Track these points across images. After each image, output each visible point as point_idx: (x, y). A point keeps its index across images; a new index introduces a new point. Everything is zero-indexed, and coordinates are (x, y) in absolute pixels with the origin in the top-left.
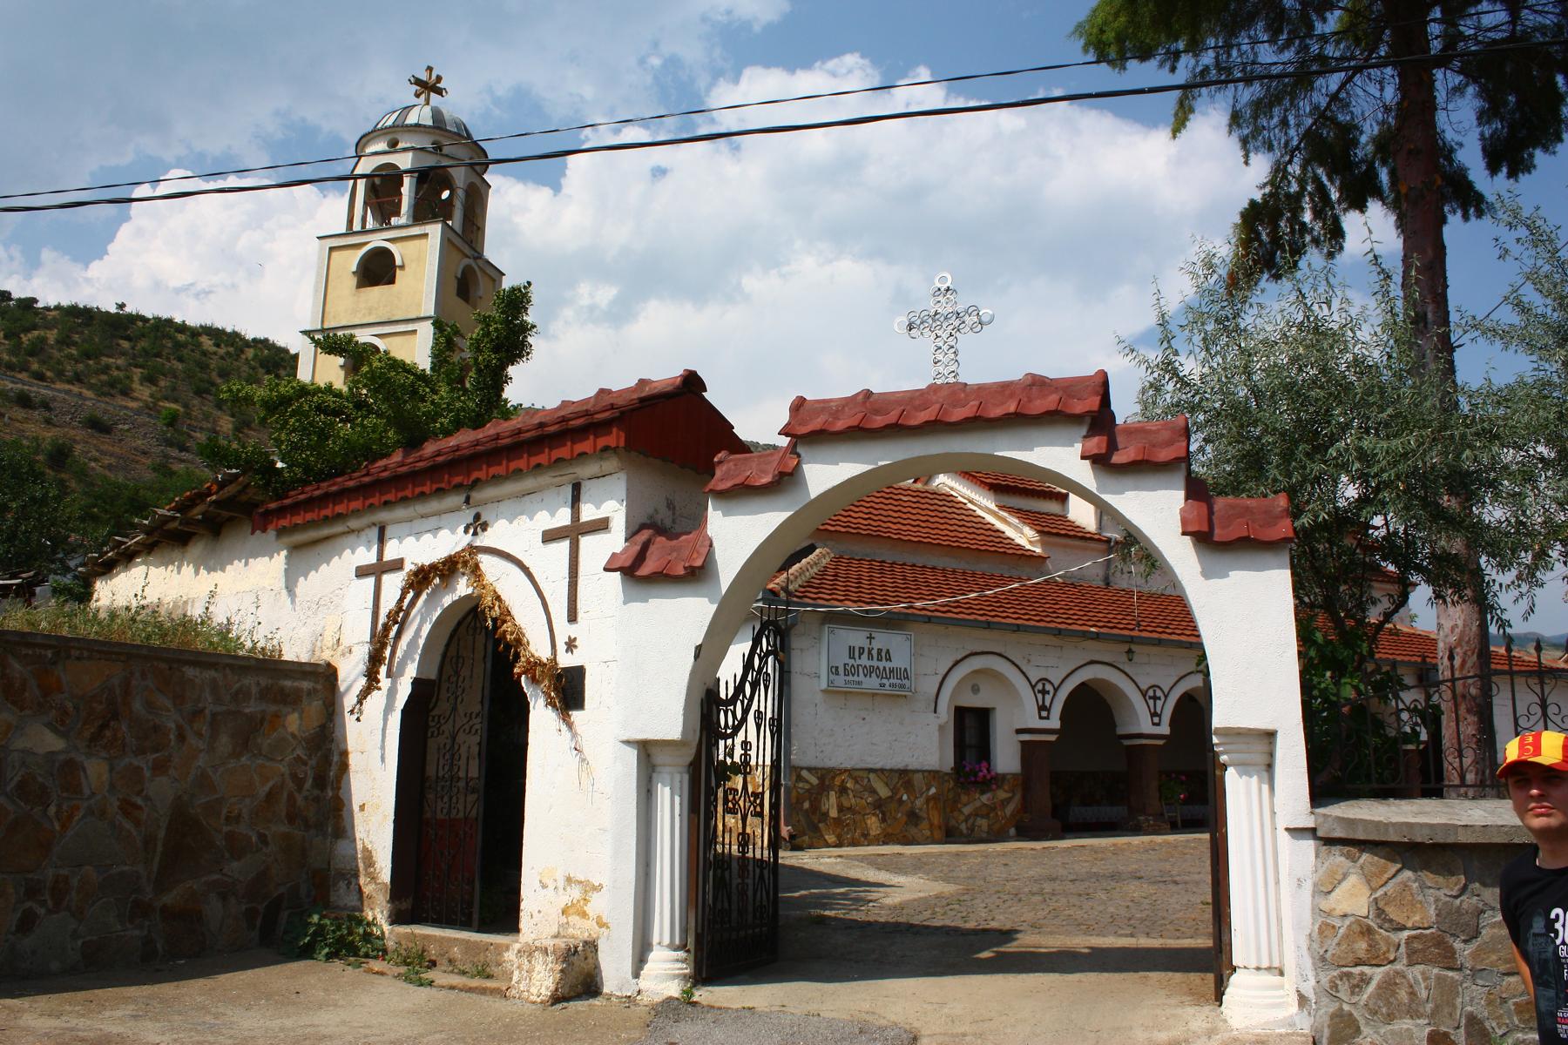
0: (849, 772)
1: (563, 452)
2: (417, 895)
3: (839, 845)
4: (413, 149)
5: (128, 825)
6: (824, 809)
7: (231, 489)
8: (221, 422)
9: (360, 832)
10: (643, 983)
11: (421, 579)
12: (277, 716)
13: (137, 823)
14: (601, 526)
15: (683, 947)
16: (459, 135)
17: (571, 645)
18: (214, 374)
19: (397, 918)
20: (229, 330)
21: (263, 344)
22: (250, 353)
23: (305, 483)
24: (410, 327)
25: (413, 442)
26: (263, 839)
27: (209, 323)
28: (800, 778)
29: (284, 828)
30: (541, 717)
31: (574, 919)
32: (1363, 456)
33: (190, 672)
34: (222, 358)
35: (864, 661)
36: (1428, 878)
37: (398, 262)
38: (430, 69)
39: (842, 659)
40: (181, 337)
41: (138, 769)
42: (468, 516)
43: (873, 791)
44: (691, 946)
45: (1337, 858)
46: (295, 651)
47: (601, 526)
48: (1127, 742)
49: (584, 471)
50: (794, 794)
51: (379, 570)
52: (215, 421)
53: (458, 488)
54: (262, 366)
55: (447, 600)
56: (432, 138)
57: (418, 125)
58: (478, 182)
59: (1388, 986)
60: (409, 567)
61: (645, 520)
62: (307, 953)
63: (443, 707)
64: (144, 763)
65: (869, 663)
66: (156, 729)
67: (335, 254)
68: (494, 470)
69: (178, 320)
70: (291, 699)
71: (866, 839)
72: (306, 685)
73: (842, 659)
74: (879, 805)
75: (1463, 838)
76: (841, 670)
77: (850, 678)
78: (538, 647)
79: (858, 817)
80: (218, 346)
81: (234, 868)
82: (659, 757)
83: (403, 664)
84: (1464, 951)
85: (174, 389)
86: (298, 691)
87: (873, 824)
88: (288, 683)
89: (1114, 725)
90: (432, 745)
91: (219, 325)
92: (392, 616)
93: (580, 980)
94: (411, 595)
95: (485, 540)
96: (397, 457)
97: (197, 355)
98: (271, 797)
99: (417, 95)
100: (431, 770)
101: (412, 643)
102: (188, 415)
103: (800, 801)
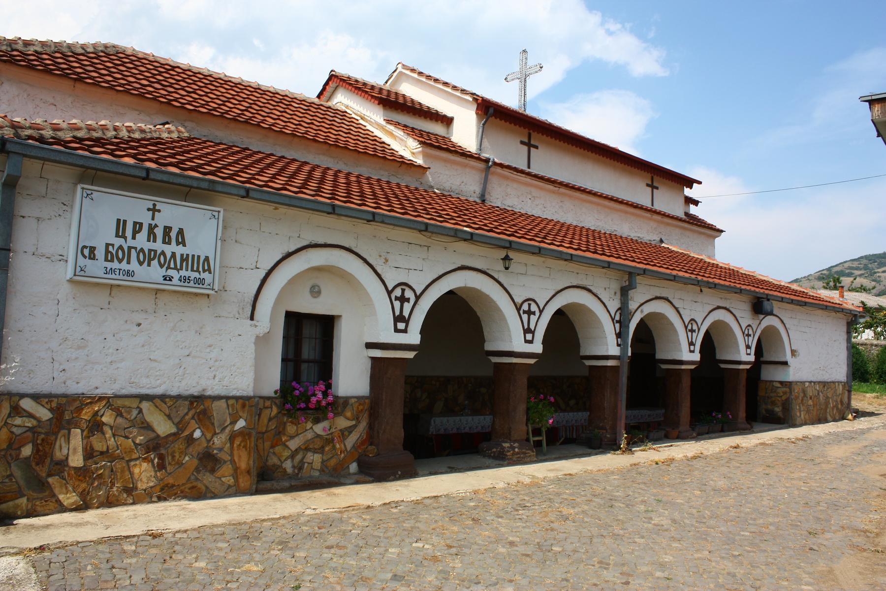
0: (108, 401)
3: (83, 507)
6: (59, 455)
28: (16, 410)
39: (105, 235)
43: (147, 427)
65: (148, 246)
73: (105, 235)
74: (155, 447)
76: (100, 253)
77: (115, 265)
79: (118, 465)
87: (144, 473)
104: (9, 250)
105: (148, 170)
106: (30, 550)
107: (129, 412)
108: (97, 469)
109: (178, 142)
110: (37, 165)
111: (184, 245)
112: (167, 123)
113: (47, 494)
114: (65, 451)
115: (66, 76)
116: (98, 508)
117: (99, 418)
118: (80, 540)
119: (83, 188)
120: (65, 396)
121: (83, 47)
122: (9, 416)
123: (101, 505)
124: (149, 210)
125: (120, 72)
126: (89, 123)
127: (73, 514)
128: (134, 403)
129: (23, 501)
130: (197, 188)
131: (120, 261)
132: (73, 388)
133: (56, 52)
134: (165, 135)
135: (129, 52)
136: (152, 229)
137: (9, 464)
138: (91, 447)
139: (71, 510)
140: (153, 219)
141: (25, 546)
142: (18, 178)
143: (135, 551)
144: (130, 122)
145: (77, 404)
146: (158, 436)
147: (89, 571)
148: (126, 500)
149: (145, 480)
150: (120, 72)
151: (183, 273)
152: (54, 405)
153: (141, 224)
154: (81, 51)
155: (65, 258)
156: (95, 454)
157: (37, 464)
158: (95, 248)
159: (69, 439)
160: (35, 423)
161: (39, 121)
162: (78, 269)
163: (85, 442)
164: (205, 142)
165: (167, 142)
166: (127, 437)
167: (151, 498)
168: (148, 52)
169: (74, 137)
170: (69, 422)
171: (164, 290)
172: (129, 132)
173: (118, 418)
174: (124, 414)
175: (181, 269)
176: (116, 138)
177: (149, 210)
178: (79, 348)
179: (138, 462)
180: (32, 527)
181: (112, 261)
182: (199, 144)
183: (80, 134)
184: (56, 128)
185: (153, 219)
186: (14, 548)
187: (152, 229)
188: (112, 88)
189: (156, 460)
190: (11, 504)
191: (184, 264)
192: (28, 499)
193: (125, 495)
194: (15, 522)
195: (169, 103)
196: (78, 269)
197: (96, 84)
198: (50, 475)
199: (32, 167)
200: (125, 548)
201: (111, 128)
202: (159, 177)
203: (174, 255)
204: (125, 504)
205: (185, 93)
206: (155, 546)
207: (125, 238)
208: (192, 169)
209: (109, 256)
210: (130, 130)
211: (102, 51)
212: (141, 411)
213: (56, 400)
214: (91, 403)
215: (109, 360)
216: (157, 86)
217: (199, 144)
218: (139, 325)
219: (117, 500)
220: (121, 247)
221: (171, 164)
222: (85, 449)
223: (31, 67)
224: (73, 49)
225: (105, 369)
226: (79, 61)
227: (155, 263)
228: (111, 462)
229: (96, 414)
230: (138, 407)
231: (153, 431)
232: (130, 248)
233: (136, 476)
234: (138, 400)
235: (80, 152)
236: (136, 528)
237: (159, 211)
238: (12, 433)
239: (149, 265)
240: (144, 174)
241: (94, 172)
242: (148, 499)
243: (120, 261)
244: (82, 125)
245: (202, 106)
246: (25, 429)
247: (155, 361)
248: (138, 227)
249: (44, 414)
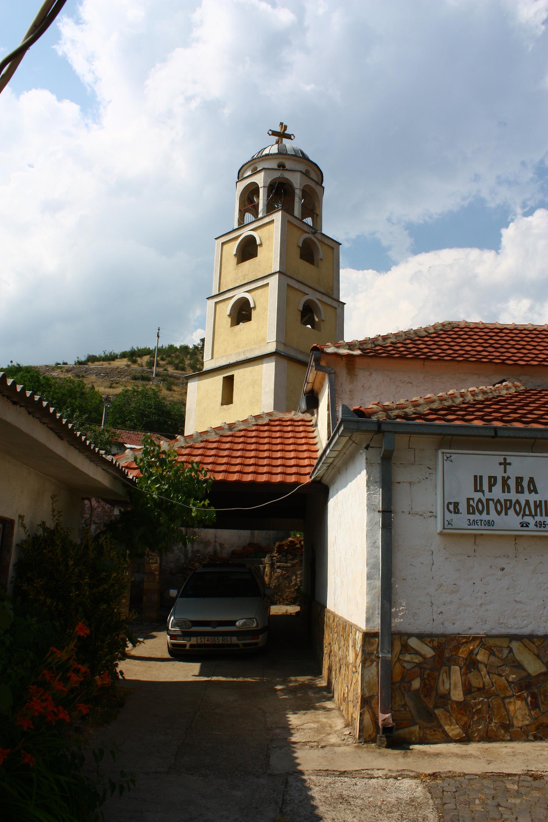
0: (483, 641)
3: (465, 739)
4: (264, 169)
6: (442, 689)
16: (297, 156)
28: (406, 648)
32: (461, 784)
35: (497, 493)
37: (258, 242)
39: (465, 491)
43: (518, 666)
50: (397, 669)
65: (503, 497)
67: (225, 247)
73: (465, 491)
74: (527, 685)
76: (463, 507)
77: (477, 516)
79: (495, 702)
87: (519, 711)
103: (406, 677)
104: (391, 512)
105: (496, 429)
106: (426, 776)
107: (501, 651)
108: (476, 705)
109: (516, 396)
110: (406, 438)
111: (536, 493)
112: (504, 381)
113: (435, 724)
114: (447, 686)
115: (416, 358)
116: (479, 741)
117: (474, 656)
118: (466, 772)
119: (443, 453)
120: (444, 636)
121: (426, 330)
122: (401, 653)
123: (482, 739)
124: (500, 464)
125: (458, 344)
126: (440, 394)
127: (458, 745)
128: (504, 643)
129: (416, 728)
130: (541, 438)
131: (481, 513)
132: (451, 629)
133: (406, 339)
134: (504, 392)
135: (462, 325)
136: (505, 481)
137: (403, 694)
138: (470, 684)
139: (456, 741)
140: (505, 472)
141: (421, 771)
142: (392, 452)
143: (517, 791)
144: (471, 387)
145: (455, 643)
146: (529, 675)
147: (477, 806)
148: (504, 736)
149: (520, 717)
150: (458, 344)
151: (538, 518)
152: (435, 644)
153: (495, 478)
154: (425, 334)
155: (434, 514)
156: (473, 690)
157: (425, 696)
158: (458, 503)
159: (450, 675)
160: (421, 659)
161: (402, 401)
162: (446, 523)
163: (464, 678)
164: (540, 392)
165: (508, 398)
166: (500, 675)
167: (528, 736)
168: (477, 321)
169: (430, 409)
170: (449, 659)
171: (522, 536)
172: (473, 395)
173: (491, 657)
174: (496, 653)
175: (536, 515)
176: (463, 403)
177: (500, 464)
178: (453, 592)
179: (512, 700)
180: (425, 754)
181: (474, 513)
182: (535, 395)
183: (435, 406)
184: (416, 404)
185: (505, 472)
186: (412, 771)
187: (505, 481)
188: (453, 360)
189: (529, 699)
190: (406, 730)
191: (538, 510)
192: (420, 728)
193: (503, 732)
194: (411, 747)
195: (503, 363)
196: (446, 523)
197: (441, 360)
198: (436, 707)
199: (402, 440)
200: (508, 786)
201: (458, 395)
202: (506, 433)
203: (527, 502)
204: (503, 740)
205: (515, 351)
206: (537, 789)
207: (483, 492)
208: (535, 421)
209: (471, 510)
210: (473, 394)
211: (441, 330)
212: (511, 651)
213: (436, 639)
214: (466, 642)
215: (479, 602)
216: (490, 349)
217: (535, 395)
218: (503, 569)
219: (496, 736)
220: (480, 500)
221: (515, 420)
222: (464, 685)
223: (390, 357)
224: (419, 334)
225: (476, 611)
226: (424, 343)
227: (511, 512)
228: (488, 698)
229: (471, 652)
230: (508, 647)
231: (524, 669)
232: (488, 500)
233: (512, 714)
234: (507, 640)
235: (437, 422)
236: (515, 767)
237: (510, 464)
238: (404, 667)
239: (506, 514)
240: (492, 433)
241: (451, 437)
242: (525, 737)
243: (481, 513)
244: (435, 398)
245: (533, 359)
246: (413, 665)
247: (520, 602)
248: (493, 481)
249: (428, 652)
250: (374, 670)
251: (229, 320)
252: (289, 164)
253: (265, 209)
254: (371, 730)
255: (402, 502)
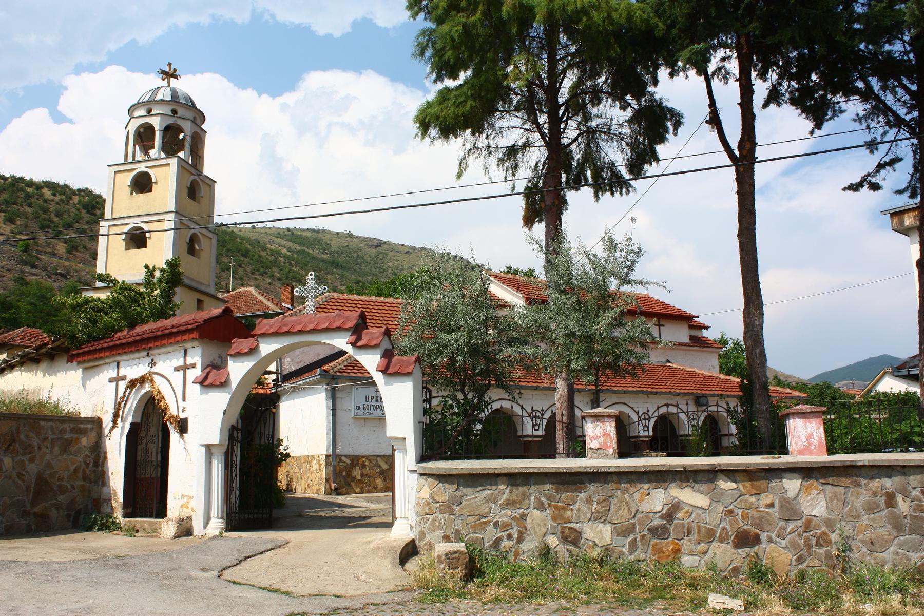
1: (179, 339)
2: (133, 507)
3: (362, 493)
5: (20, 482)
6: (354, 475)
7: (58, 343)
8: (58, 248)
9: (112, 484)
10: (207, 531)
11: (132, 384)
12: (77, 439)
13: (23, 481)
14: (193, 366)
15: (222, 518)
17: (184, 410)
18: (53, 214)
19: (126, 515)
20: (61, 183)
21: (85, 192)
22: (76, 199)
23: (88, 342)
24: (161, 217)
25: (132, 326)
26: (73, 487)
27: (48, 179)
28: (341, 460)
29: (81, 483)
30: (174, 436)
31: (185, 509)
33: (42, 423)
34: (58, 203)
36: (447, 485)
37: (154, 180)
38: (170, 64)
40: (30, 190)
41: (23, 461)
42: (149, 360)
43: (380, 466)
44: (225, 516)
45: (422, 480)
46: (85, 413)
47: (193, 366)
48: (633, 440)
49: (188, 345)
51: (117, 380)
52: (54, 247)
53: (144, 349)
54: (84, 208)
55: (142, 392)
56: (171, 108)
57: (163, 100)
58: (199, 131)
59: (434, 521)
60: (128, 379)
61: (209, 363)
62: (90, 529)
63: (143, 434)
64: (25, 459)
65: (376, 404)
66: (30, 445)
67: (117, 175)
68: (156, 344)
69: (28, 178)
70: (84, 432)
71: (376, 489)
72: (89, 426)
75: (454, 472)
78: (173, 411)
80: (54, 195)
81: (62, 498)
82: (213, 450)
83: (127, 417)
84: (456, 509)
85: (26, 226)
86: (86, 429)
88: (82, 426)
89: (516, 431)
90: (139, 447)
91: (55, 180)
92: (122, 399)
93: (185, 530)
94: (129, 390)
95: (154, 369)
96: (125, 333)
97: (41, 202)
98: (76, 470)
99: (163, 80)
100: (139, 458)
101: (130, 409)
102: (36, 244)
103: (341, 471)
250: (331, 468)
251: (124, 244)
252: (181, 112)
253: (573, 487)
254: (329, 491)
255: (338, 406)
